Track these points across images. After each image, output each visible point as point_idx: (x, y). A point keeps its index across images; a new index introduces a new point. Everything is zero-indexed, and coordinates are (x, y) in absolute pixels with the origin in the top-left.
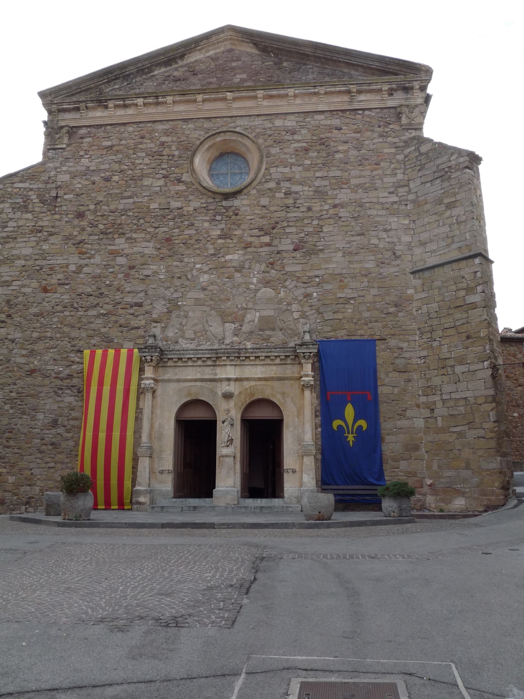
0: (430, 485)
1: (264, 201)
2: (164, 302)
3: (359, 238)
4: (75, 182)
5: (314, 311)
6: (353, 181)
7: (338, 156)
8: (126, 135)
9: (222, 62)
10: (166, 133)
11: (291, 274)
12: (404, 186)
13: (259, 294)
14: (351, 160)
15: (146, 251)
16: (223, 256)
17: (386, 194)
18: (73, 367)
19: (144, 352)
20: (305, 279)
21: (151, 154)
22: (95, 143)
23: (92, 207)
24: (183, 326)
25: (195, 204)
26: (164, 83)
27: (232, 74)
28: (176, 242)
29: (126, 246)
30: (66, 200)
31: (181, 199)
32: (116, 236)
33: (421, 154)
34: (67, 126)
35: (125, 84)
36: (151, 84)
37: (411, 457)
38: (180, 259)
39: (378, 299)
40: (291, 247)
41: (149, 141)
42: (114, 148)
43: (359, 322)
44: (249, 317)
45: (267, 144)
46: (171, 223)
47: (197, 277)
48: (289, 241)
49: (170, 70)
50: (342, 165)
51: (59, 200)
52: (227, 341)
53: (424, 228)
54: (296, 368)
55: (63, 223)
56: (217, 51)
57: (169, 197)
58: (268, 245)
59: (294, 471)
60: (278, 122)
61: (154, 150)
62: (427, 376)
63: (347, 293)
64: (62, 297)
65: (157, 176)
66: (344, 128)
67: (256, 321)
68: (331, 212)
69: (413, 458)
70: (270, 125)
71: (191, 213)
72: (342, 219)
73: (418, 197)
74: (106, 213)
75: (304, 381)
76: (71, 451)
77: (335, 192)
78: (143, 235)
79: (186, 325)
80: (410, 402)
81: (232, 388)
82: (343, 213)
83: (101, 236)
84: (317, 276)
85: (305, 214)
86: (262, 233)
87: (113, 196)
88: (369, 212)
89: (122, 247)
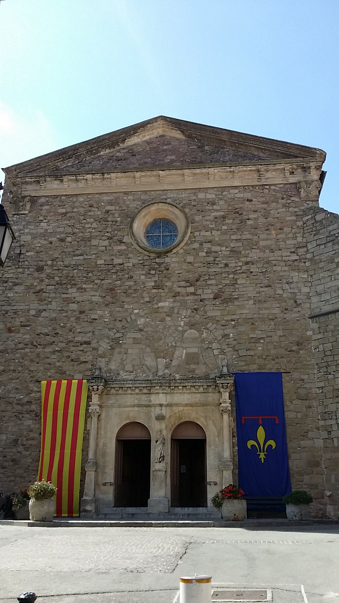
0: (330, 496)
1: (190, 259)
2: (108, 341)
3: (267, 289)
4: (35, 242)
5: (231, 349)
6: (262, 243)
7: (249, 222)
8: (77, 204)
9: (155, 145)
10: (110, 203)
11: (212, 318)
12: (303, 247)
13: (186, 335)
14: (260, 226)
15: (94, 299)
16: (156, 304)
17: (289, 254)
18: (33, 395)
19: (91, 383)
20: (223, 322)
21: (98, 220)
22: (52, 211)
23: (49, 263)
24: (124, 361)
25: (134, 261)
26: (109, 162)
27: (164, 155)
28: (118, 291)
29: (78, 294)
30: (28, 256)
31: (122, 257)
32: (69, 286)
33: (316, 222)
34: (29, 196)
35: (77, 162)
36: (98, 162)
37: (313, 472)
38: (121, 305)
39: (283, 339)
40: (212, 296)
41: (97, 209)
42: (68, 215)
43: (268, 358)
44: (177, 353)
45: (192, 212)
46: (114, 276)
47: (136, 320)
48: (210, 291)
49: (113, 151)
50: (253, 230)
51: (22, 256)
52: (160, 373)
53: (319, 281)
54: (216, 395)
55: (26, 275)
56: (152, 136)
57: (112, 255)
58: (194, 294)
59: (216, 484)
60: (201, 195)
61: (101, 217)
62: (325, 404)
63: (258, 334)
64: (24, 337)
65: (103, 238)
66: (254, 200)
67: (183, 357)
68: (244, 268)
69: (315, 473)
70: (195, 198)
71: (131, 268)
72: (253, 274)
73: (314, 257)
74: (61, 268)
75: (223, 407)
76: (29, 466)
77: (247, 252)
78: (91, 286)
79: (126, 360)
80: (311, 426)
81: (164, 411)
82: (253, 268)
83: (57, 286)
84: (232, 320)
85: (223, 270)
86: (188, 284)
87: (67, 253)
88: (275, 268)
89: (74, 295)
